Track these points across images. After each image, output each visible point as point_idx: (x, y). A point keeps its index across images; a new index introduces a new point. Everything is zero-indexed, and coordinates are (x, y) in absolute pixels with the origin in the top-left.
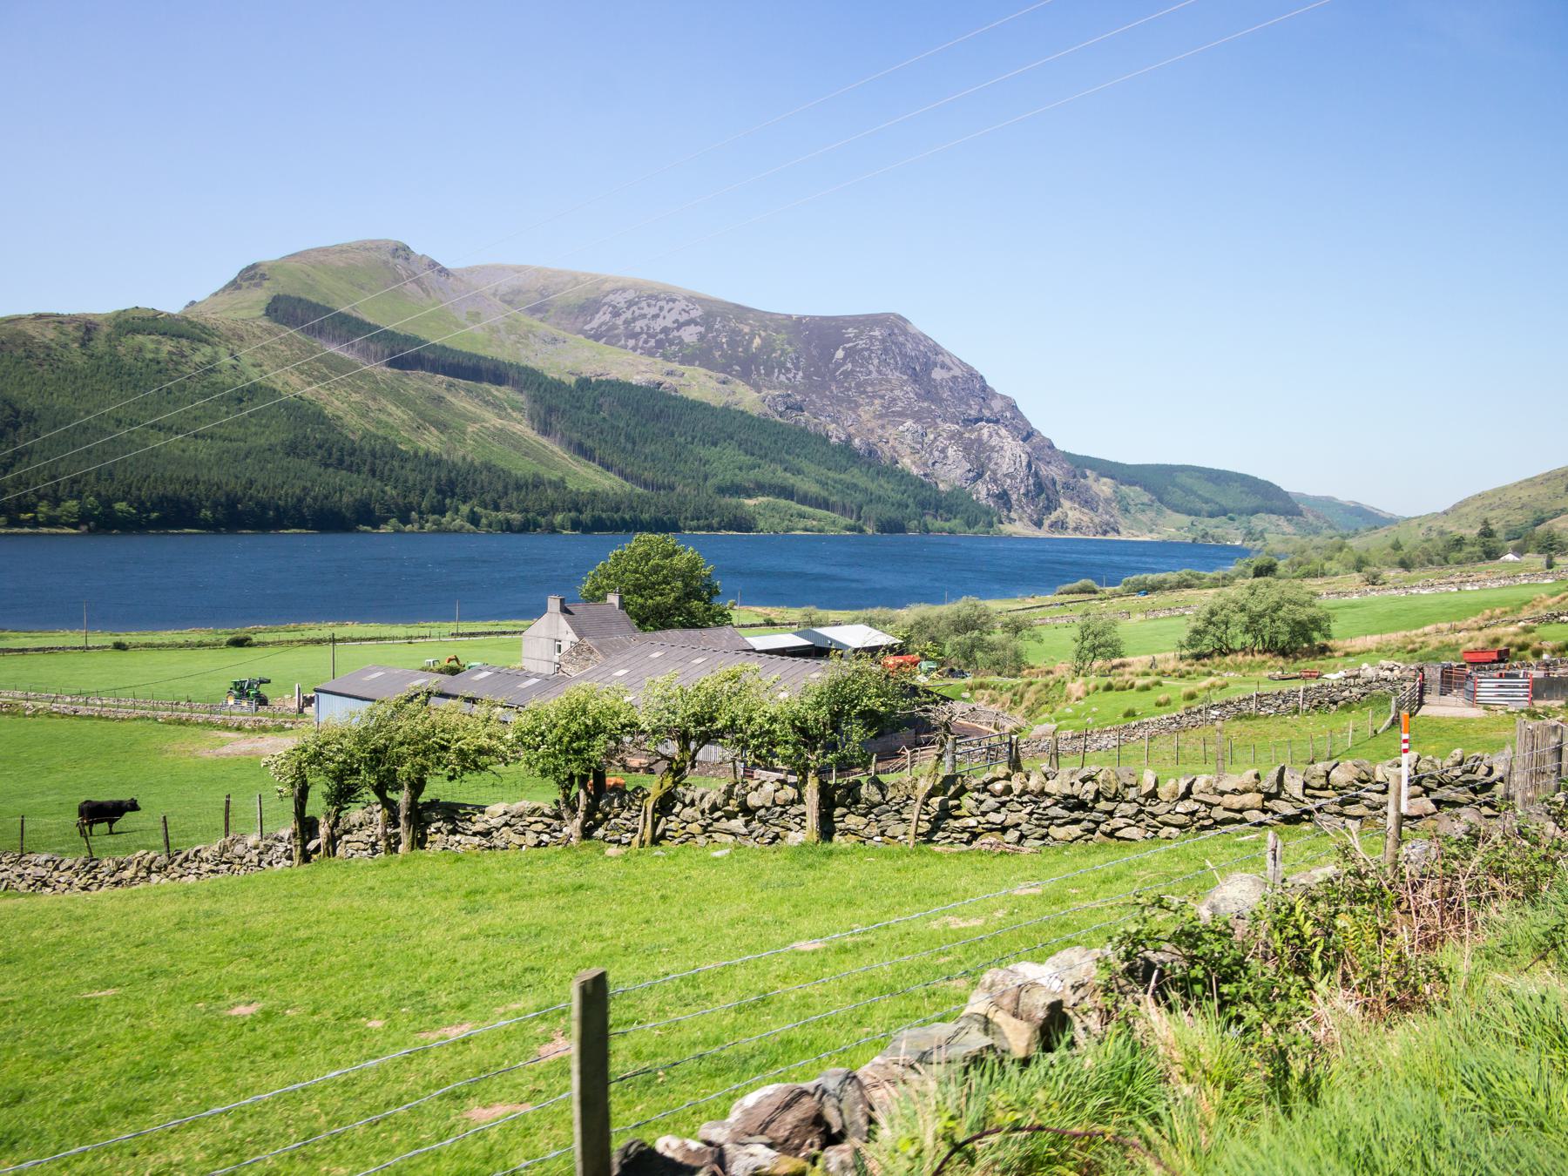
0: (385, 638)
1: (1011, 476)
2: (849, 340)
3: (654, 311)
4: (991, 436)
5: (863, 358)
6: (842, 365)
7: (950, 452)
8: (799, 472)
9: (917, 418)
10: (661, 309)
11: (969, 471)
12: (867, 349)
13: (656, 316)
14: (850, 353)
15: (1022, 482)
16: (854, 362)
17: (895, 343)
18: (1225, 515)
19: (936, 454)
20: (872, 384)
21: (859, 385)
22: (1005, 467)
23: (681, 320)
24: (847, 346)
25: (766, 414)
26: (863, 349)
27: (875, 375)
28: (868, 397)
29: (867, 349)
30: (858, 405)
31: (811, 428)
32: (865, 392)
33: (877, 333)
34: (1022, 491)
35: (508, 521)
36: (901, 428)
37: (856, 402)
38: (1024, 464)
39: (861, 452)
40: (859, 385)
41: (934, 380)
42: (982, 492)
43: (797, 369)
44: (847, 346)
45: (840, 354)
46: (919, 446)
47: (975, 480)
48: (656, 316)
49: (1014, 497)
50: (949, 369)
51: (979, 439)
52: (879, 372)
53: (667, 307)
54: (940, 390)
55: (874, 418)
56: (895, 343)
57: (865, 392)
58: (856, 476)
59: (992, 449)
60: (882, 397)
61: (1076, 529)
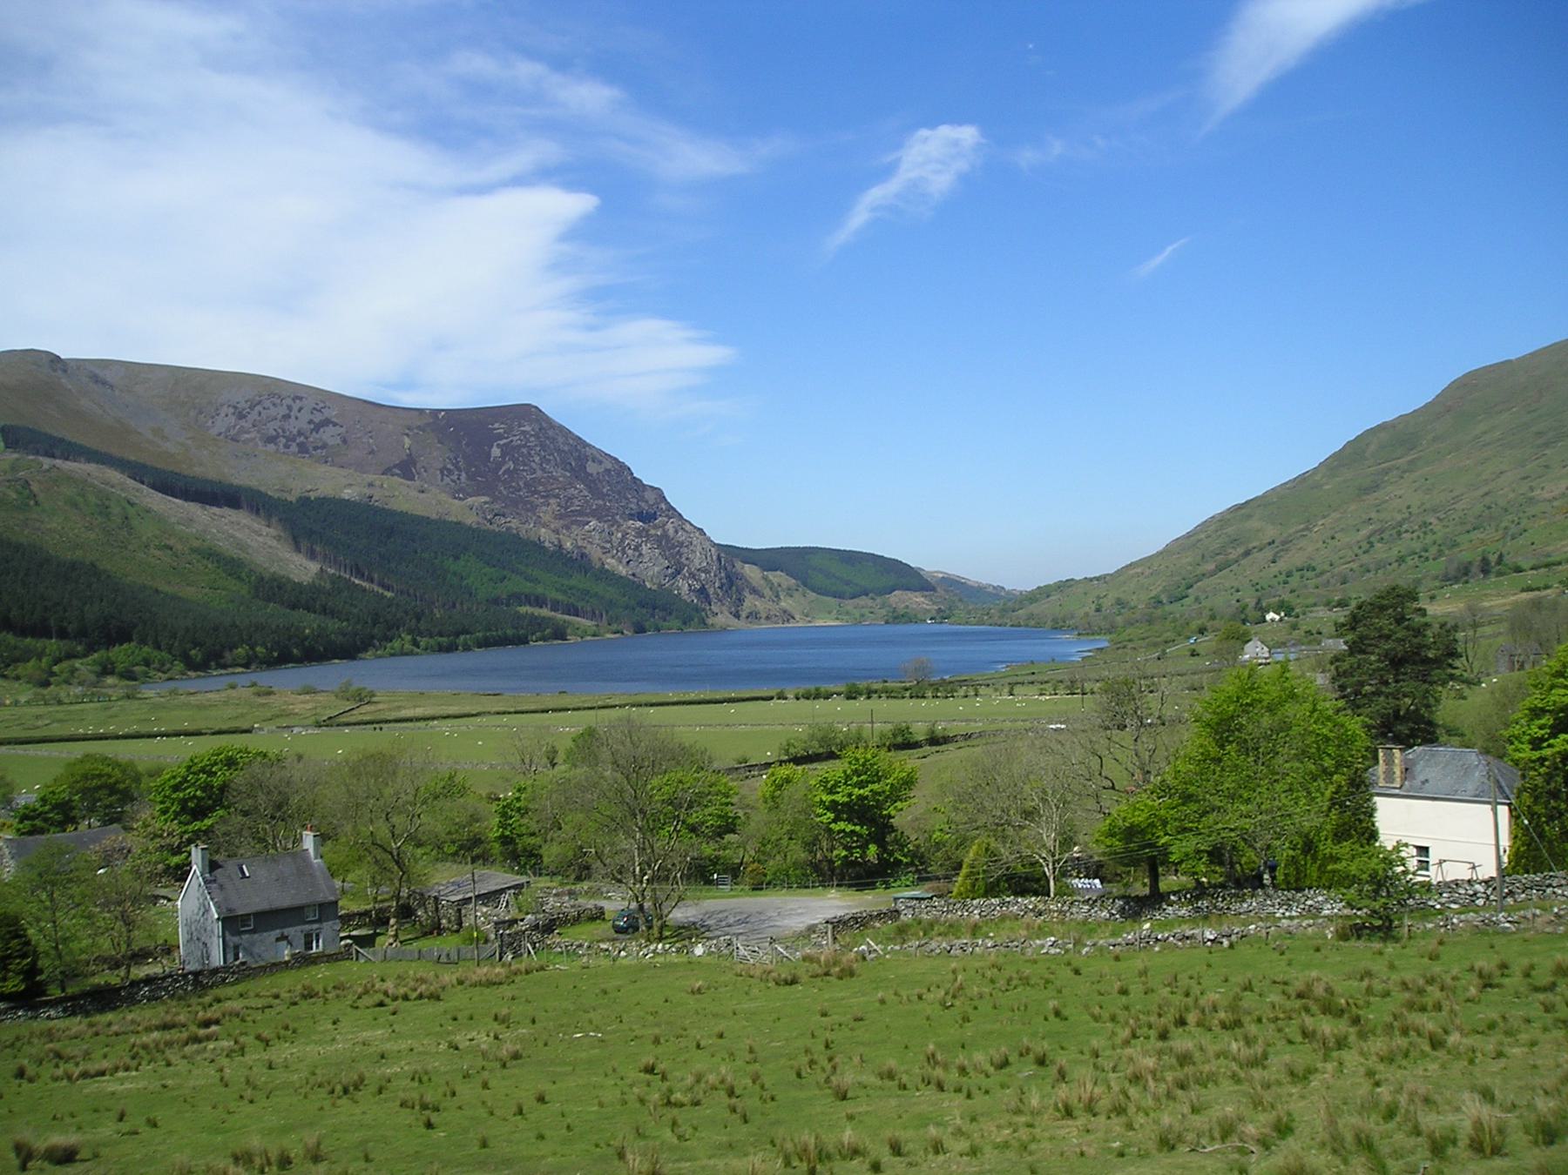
0: (615, 706)
1: (707, 571)
2: (500, 437)
3: (283, 411)
4: (676, 532)
5: (522, 455)
6: (504, 463)
7: (644, 549)
8: (536, 581)
9: (598, 514)
10: (289, 408)
11: (668, 567)
12: (525, 446)
13: (286, 417)
14: (507, 450)
15: (715, 576)
16: (515, 461)
17: (548, 438)
18: (867, 595)
19: (630, 552)
20: (541, 483)
21: (527, 485)
22: (697, 562)
23: (317, 420)
24: (501, 442)
25: (478, 523)
26: (520, 446)
27: (539, 473)
28: (543, 497)
29: (525, 446)
30: (533, 508)
31: (523, 534)
32: (536, 492)
33: (527, 428)
34: (717, 585)
35: (439, 644)
36: (587, 527)
37: (531, 503)
38: (715, 558)
39: (575, 556)
40: (527, 485)
41: (591, 475)
42: (683, 586)
43: (459, 469)
44: (501, 442)
45: (496, 452)
46: (608, 545)
47: (674, 576)
48: (286, 417)
49: (711, 591)
50: (601, 462)
51: (665, 535)
52: (543, 470)
53: (295, 408)
54: (599, 485)
55: (555, 518)
56: (548, 438)
57: (536, 492)
58: (577, 580)
59: (681, 544)
60: (557, 496)
61: (767, 618)
